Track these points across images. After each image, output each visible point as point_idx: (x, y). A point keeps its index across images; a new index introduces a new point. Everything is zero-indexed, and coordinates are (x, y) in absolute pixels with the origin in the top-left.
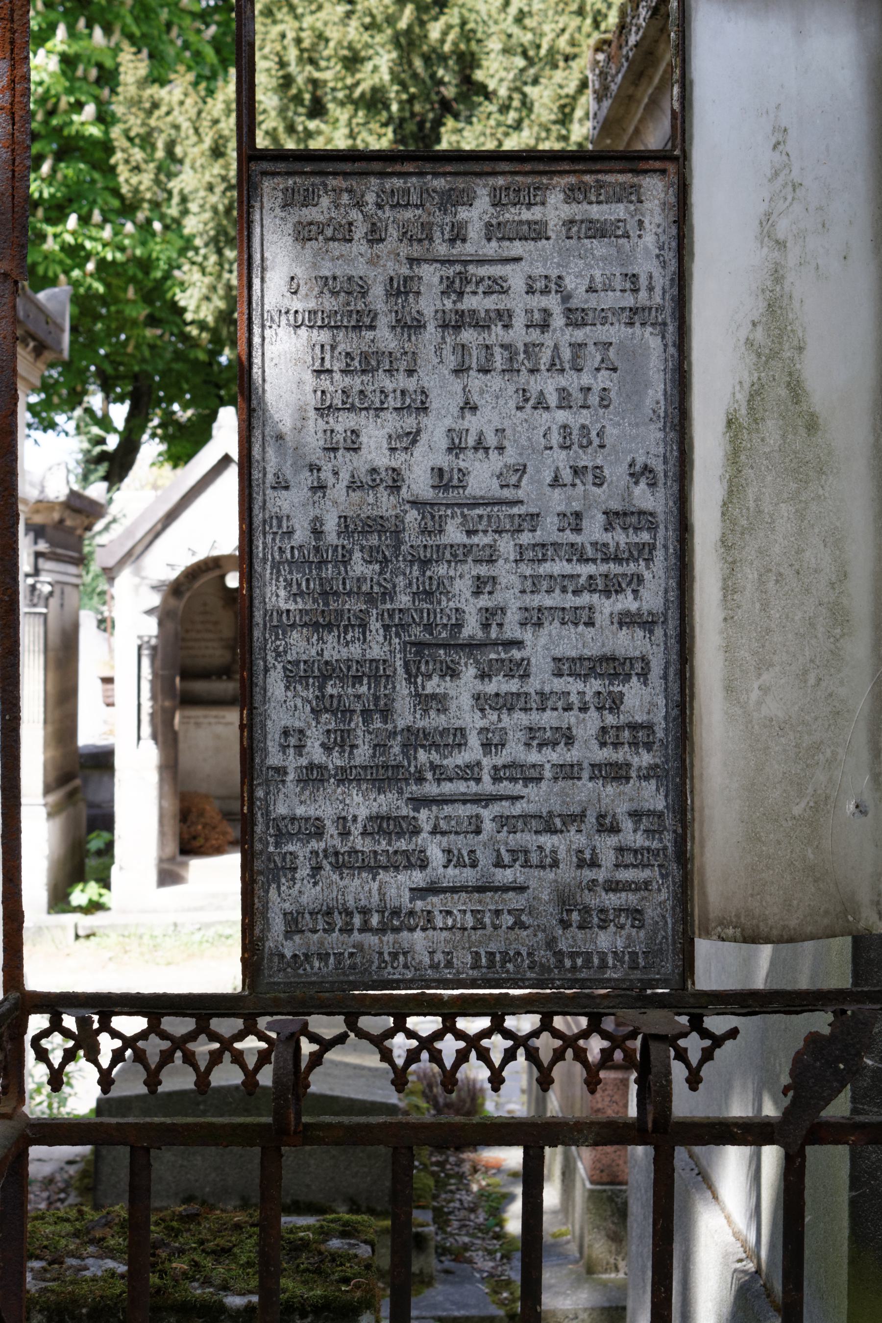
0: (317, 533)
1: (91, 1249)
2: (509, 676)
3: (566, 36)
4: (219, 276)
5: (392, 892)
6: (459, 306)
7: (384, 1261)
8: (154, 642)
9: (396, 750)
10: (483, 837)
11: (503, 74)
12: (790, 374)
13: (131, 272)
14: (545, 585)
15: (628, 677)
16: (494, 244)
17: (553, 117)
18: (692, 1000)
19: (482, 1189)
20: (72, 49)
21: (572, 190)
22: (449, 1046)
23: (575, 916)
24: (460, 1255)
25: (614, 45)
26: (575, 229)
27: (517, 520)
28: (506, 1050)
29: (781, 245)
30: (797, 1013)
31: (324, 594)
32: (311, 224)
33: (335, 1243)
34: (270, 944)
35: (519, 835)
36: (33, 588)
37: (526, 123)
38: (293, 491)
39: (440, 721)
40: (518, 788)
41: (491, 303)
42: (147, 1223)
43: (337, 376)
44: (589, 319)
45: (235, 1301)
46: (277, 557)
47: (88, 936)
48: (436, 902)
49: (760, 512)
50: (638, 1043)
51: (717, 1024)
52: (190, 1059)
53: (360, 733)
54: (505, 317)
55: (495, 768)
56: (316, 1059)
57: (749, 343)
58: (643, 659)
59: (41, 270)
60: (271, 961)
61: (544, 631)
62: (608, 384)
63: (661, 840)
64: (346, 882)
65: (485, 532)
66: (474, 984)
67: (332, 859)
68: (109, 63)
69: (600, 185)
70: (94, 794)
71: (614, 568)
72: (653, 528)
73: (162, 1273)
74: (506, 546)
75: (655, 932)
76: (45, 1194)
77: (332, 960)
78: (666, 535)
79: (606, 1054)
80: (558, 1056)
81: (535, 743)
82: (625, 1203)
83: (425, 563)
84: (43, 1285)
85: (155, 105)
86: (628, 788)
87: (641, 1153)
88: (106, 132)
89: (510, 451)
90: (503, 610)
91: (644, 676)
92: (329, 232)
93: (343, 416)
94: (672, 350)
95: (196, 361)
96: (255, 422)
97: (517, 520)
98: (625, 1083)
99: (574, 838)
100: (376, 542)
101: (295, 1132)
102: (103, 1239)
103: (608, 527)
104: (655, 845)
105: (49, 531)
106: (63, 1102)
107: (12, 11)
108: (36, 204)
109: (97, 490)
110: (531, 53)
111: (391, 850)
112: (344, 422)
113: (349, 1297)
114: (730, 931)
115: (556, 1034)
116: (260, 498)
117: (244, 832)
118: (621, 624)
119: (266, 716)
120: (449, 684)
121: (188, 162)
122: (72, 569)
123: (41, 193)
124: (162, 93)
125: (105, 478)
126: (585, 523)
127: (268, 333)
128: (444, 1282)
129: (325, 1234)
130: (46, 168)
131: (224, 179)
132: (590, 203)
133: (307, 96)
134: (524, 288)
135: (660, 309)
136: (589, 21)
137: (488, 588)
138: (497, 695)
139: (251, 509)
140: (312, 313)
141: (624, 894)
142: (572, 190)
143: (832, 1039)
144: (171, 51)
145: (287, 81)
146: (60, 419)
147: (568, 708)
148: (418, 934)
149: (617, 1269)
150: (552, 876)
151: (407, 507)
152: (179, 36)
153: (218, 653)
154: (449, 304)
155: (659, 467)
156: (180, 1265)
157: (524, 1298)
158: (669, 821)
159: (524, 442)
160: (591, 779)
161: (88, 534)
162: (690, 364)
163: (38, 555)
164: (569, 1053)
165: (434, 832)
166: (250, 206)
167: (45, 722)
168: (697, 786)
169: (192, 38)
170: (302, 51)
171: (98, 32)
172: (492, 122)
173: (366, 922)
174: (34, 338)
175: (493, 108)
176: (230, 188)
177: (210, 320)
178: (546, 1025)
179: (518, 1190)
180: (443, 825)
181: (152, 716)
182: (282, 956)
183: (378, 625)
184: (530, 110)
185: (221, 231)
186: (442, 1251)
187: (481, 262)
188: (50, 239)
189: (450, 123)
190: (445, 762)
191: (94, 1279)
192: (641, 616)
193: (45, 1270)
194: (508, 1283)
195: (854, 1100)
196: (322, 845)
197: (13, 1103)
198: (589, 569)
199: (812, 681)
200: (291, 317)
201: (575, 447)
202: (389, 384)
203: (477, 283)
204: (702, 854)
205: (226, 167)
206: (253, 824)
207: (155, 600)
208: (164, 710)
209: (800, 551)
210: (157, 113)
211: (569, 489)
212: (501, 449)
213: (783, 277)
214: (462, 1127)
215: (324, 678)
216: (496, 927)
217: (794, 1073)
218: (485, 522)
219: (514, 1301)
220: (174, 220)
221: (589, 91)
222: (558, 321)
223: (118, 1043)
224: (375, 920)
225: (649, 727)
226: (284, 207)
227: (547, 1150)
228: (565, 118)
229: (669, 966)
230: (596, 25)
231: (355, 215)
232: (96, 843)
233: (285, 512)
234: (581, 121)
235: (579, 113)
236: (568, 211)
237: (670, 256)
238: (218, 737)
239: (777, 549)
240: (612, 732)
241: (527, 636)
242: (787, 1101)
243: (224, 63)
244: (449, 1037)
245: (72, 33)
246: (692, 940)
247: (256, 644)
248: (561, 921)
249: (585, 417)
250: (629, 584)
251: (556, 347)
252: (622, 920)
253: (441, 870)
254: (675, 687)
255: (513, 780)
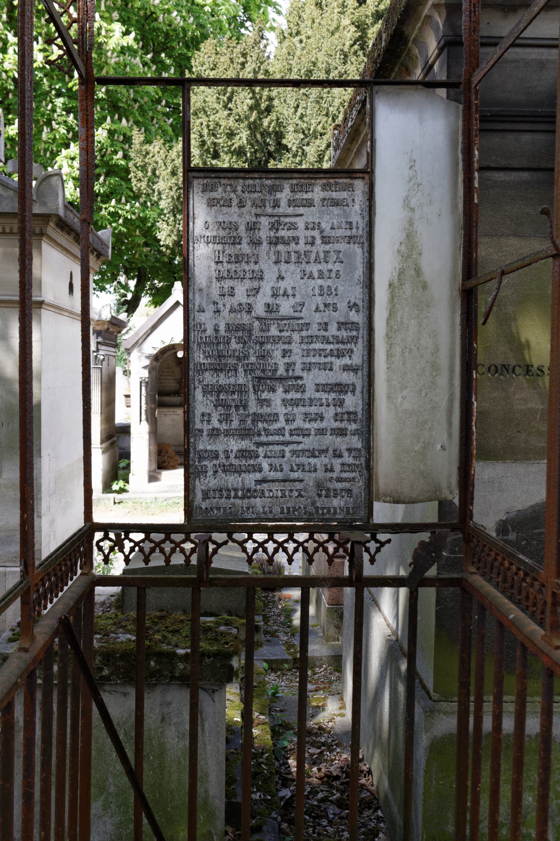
0: (216, 331)
1: (121, 630)
2: (297, 391)
3: (321, 125)
4: (175, 226)
5: (247, 482)
6: (277, 235)
7: (243, 636)
8: (147, 380)
9: (249, 422)
10: (285, 459)
11: (294, 141)
12: (416, 265)
13: (137, 224)
14: (312, 353)
15: (347, 392)
16: (291, 208)
17: (315, 159)
18: (372, 527)
19: (283, 607)
20: (114, 127)
21: (324, 185)
22: (271, 546)
23: (324, 492)
24: (273, 634)
25: (342, 127)
26: (326, 202)
27: (300, 326)
28: (294, 548)
29: (412, 210)
30: (416, 533)
31: (219, 356)
32: (214, 199)
33: (222, 628)
34: (196, 503)
35: (300, 458)
36: (96, 357)
37: (304, 161)
38: (206, 313)
39: (268, 410)
40: (300, 439)
41: (290, 233)
42: (144, 620)
43: (225, 264)
44: (332, 241)
45: (181, 652)
46: (200, 341)
47: (119, 503)
48: (265, 486)
49: (403, 323)
50: (349, 545)
51: (382, 537)
52: (162, 551)
53: (234, 415)
54: (296, 240)
55: (291, 430)
56: (215, 551)
57: (399, 251)
58: (353, 384)
59: (100, 223)
60: (196, 510)
61: (312, 373)
62: (339, 268)
63: (360, 461)
64: (228, 477)
65: (287, 331)
66: (281, 520)
67: (222, 468)
68: (129, 134)
69: (336, 184)
70: (122, 444)
71: (341, 346)
72: (357, 330)
73: (150, 640)
74: (296, 337)
75: (357, 499)
76: (101, 609)
77: (222, 510)
78: (363, 332)
79: (336, 550)
80: (316, 550)
81: (307, 420)
82: (342, 613)
83: (262, 344)
84: (101, 644)
85: (148, 153)
86: (346, 439)
87: (349, 592)
88: (127, 164)
89: (298, 296)
90: (295, 364)
91: (353, 392)
92: (222, 203)
93: (227, 281)
94: (366, 254)
95: (164, 262)
96: (190, 283)
97: (300, 326)
98: (343, 564)
99: (325, 460)
100: (241, 335)
101: (206, 581)
102: (126, 626)
103: (339, 329)
104: (357, 462)
105: (103, 333)
106: (109, 570)
107: (87, 106)
108: (97, 195)
109: (123, 316)
110: (306, 132)
111: (247, 464)
112: (227, 284)
113: (228, 650)
114: (388, 499)
115: (315, 541)
116: (192, 316)
117: (185, 460)
118: (344, 370)
119: (195, 408)
120: (271, 395)
121: (161, 177)
122: (113, 349)
123: (99, 191)
124: (150, 148)
125: (126, 311)
126: (329, 327)
127: (196, 245)
128: (267, 645)
129: (218, 624)
130: (102, 179)
131: (176, 185)
132: (332, 191)
133: (212, 150)
134: (304, 227)
135: (361, 237)
136: (330, 119)
137: (288, 355)
138: (292, 399)
139: (188, 321)
140: (215, 237)
141: (344, 483)
142: (324, 185)
143: (429, 544)
144: (153, 129)
145: (203, 143)
146: (108, 286)
147: (321, 405)
148: (258, 499)
149: (338, 640)
150: (314, 475)
151: (254, 320)
152: (157, 123)
153: (174, 385)
154: (272, 234)
155: (360, 304)
156: (158, 637)
157: (301, 652)
158: (363, 452)
159: (304, 293)
160: (331, 435)
161: (119, 335)
162: (374, 260)
163: (98, 343)
164: (321, 549)
165: (265, 457)
166: (188, 191)
167: (101, 413)
168: (375, 438)
169: (162, 123)
170: (209, 130)
171: (124, 120)
172: (290, 162)
173: (236, 494)
174: (96, 251)
175: (290, 155)
176: (179, 188)
177: (171, 244)
178: (311, 537)
179: (299, 608)
180: (269, 454)
181: (146, 411)
182: (201, 508)
183: (242, 370)
184: (306, 156)
185: (175, 207)
186: (266, 633)
187: (286, 216)
188: (104, 210)
189: (272, 162)
190: (270, 428)
191: (122, 642)
192: (352, 366)
193: (101, 638)
194: (294, 645)
195: (438, 569)
196: (218, 462)
197: (88, 569)
198: (331, 347)
199: (423, 394)
200: (206, 239)
201: (325, 295)
202: (247, 268)
203: (284, 225)
204: (377, 466)
205: (178, 180)
206: (189, 453)
207: (147, 362)
208: (151, 408)
209: (419, 340)
210: (148, 156)
211: (322, 312)
212: (294, 295)
213: (413, 224)
214: (276, 579)
215: (219, 392)
216: (290, 497)
217: (413, 558)
218: (287, 327)
219: (296, 653)
220: (155, 202)
221: (331, 148)
222: (318, 241)
223: (132, 544)
224: (240, 494)
225: (355, 413)
226: (203, 191)
227: (311, 589)
228: (320, 159)
229: (362, 513)
230: (334, 120)
231: (233, 195)
232: (122, 464)
233: (203, 322)
234: (327, 161)
235: (326, 158)
236: (323, 194)
237: (366, 214)
238: (174, 420)
239: (410, 339)
240: (340, 415)
241: (305, 375)
242: (411, 569)
243: (177, 136)
244: (271, 542)
245: (113, 121)
246: (372, 502)
247: (191, 378)
248: (318, 494)
249: (329, 282)
250: (347, 353)
251: (317, 252)
252: (343, 494)
253: (268, 473)
254: (366, 397)
255: (298, 435)
